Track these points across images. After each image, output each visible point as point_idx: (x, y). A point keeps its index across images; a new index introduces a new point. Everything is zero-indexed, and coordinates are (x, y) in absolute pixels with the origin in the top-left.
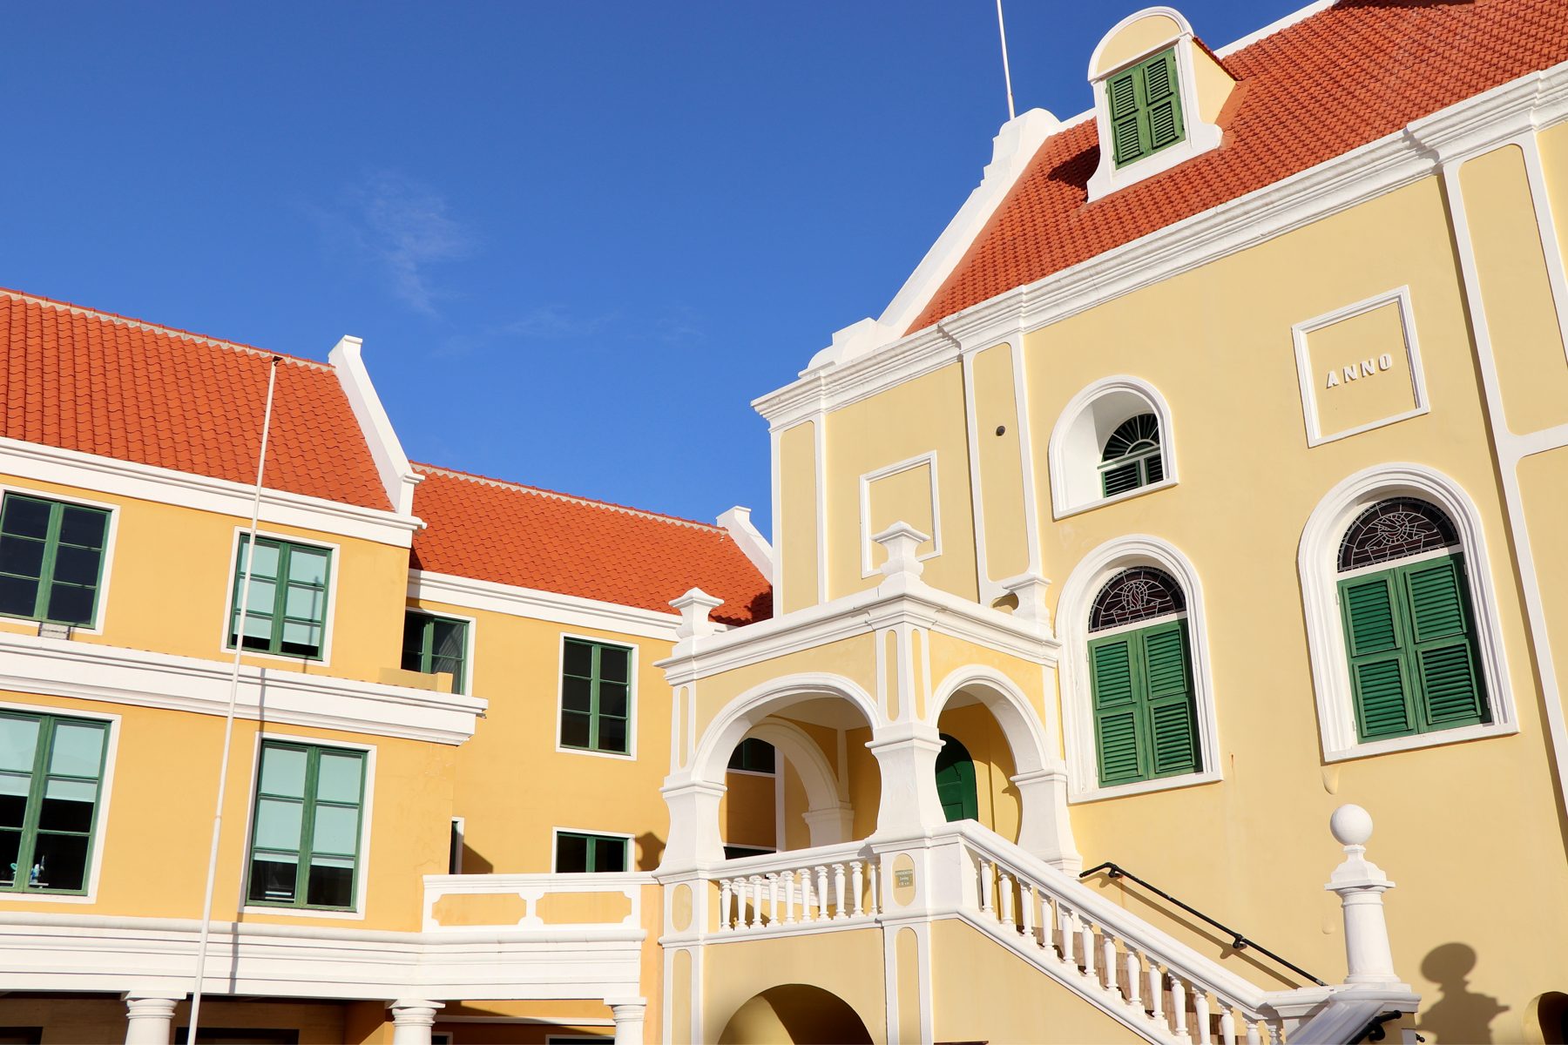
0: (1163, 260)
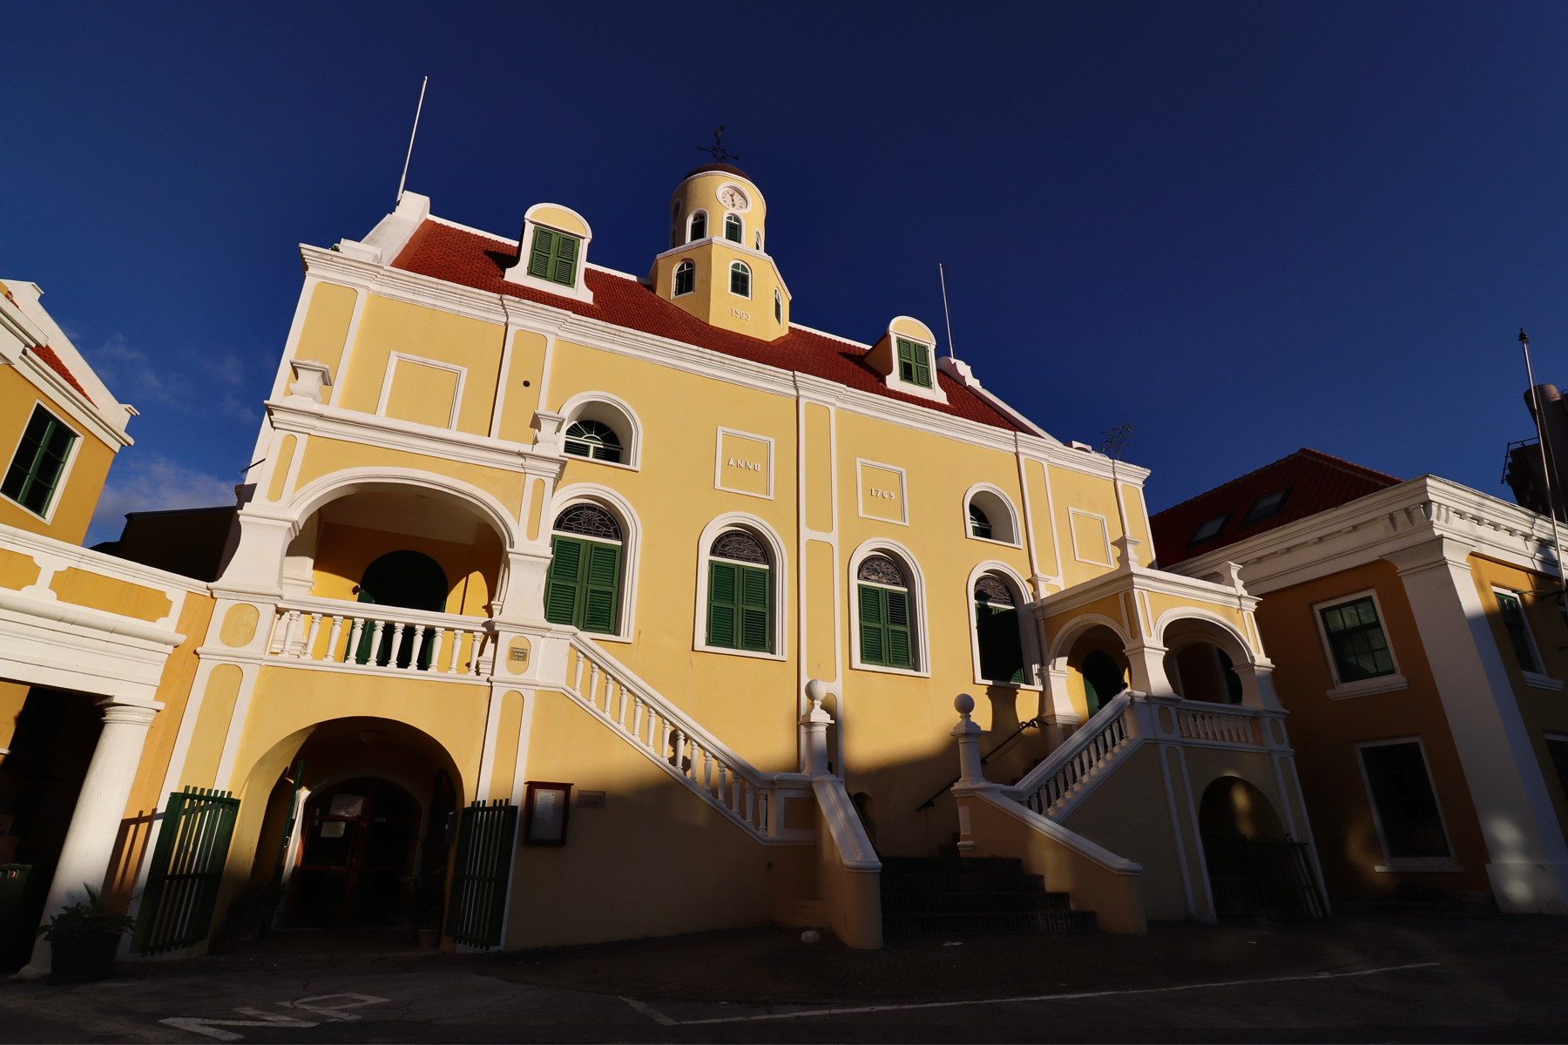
0: (657, 353)
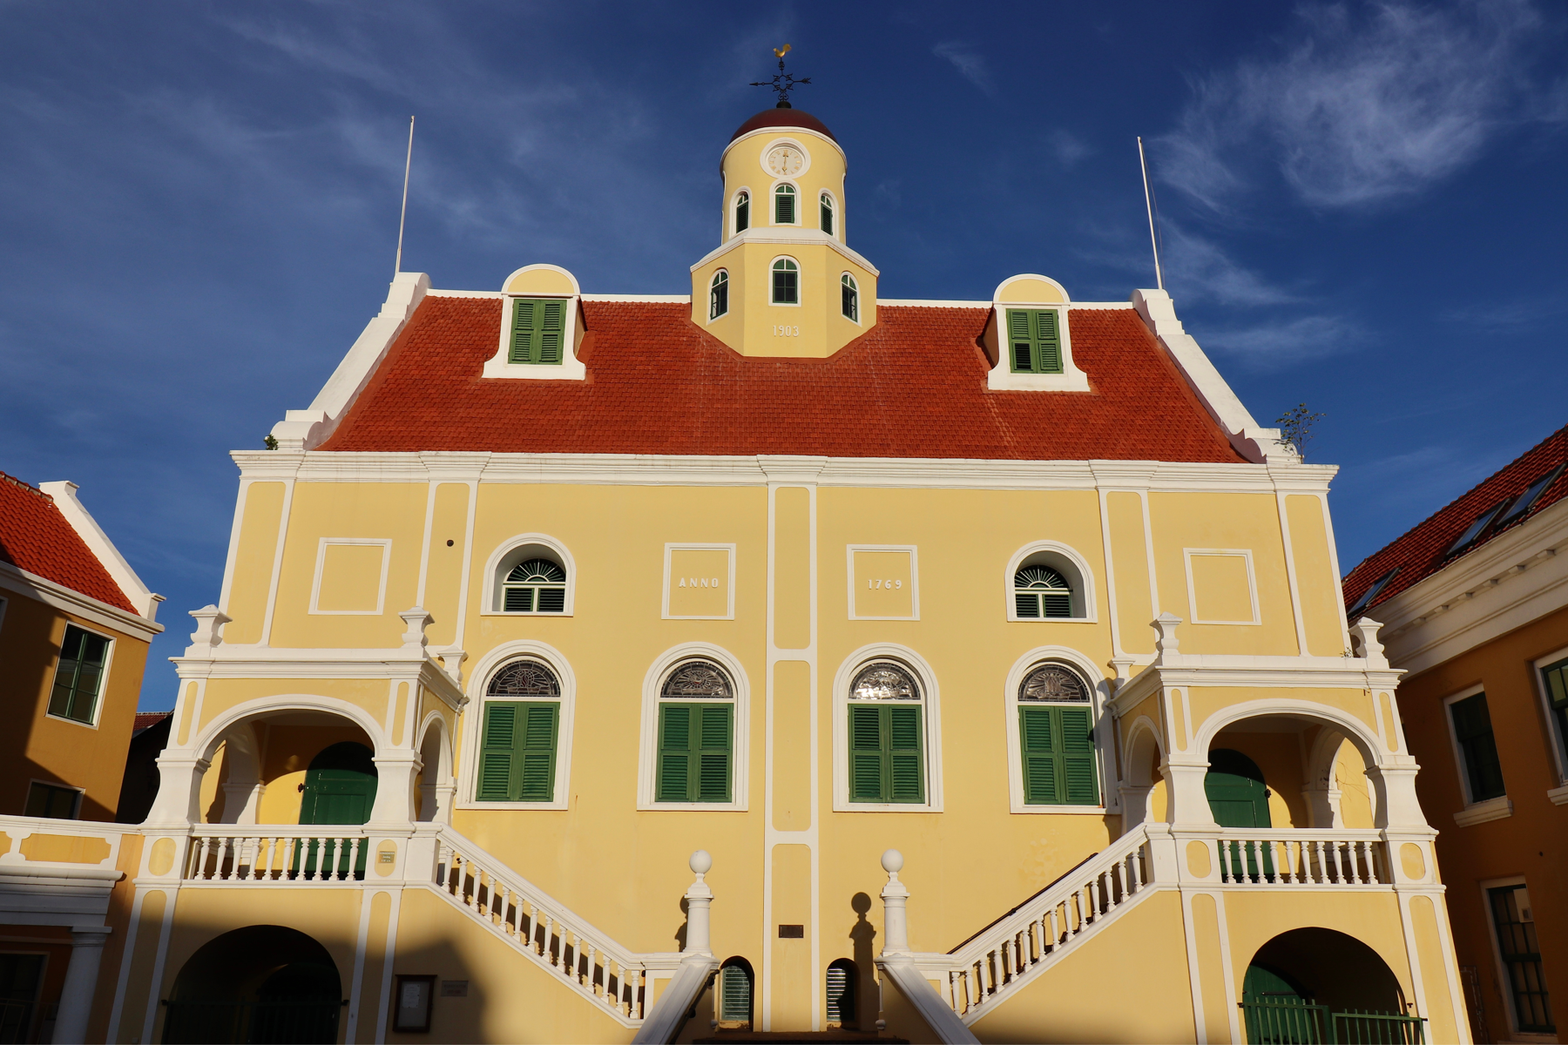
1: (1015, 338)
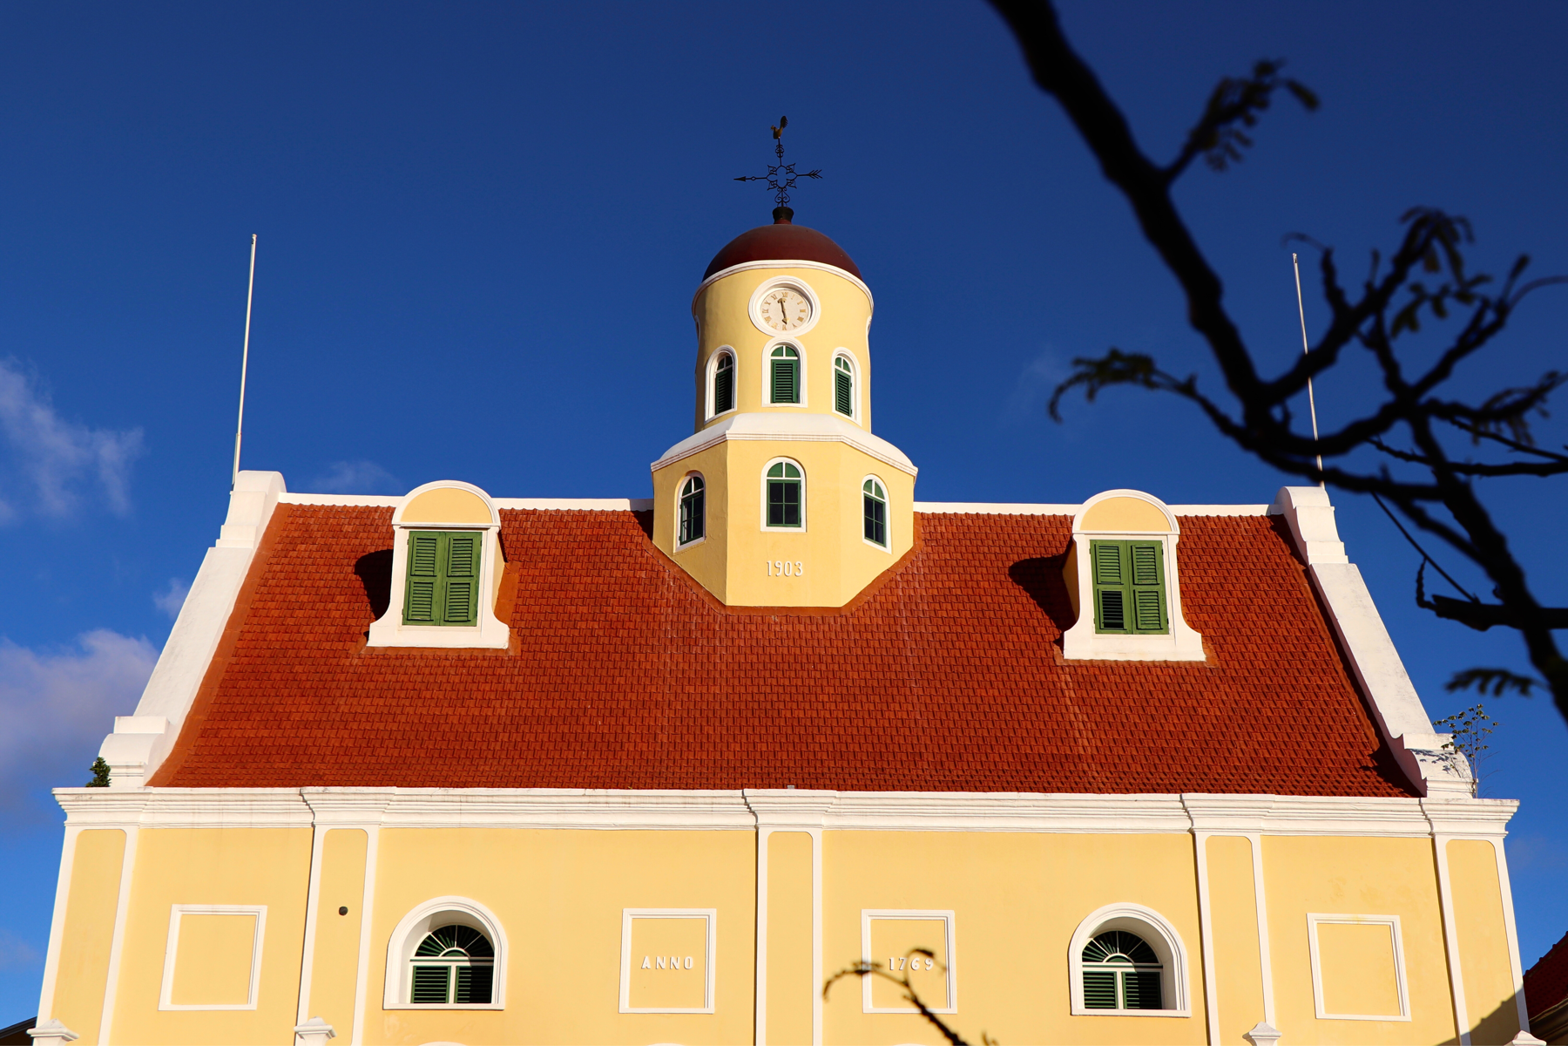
0: (527, 812)
1: (1103, 583)
